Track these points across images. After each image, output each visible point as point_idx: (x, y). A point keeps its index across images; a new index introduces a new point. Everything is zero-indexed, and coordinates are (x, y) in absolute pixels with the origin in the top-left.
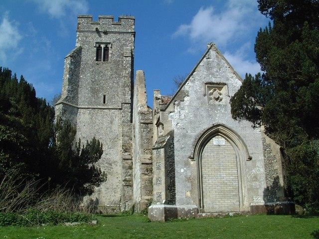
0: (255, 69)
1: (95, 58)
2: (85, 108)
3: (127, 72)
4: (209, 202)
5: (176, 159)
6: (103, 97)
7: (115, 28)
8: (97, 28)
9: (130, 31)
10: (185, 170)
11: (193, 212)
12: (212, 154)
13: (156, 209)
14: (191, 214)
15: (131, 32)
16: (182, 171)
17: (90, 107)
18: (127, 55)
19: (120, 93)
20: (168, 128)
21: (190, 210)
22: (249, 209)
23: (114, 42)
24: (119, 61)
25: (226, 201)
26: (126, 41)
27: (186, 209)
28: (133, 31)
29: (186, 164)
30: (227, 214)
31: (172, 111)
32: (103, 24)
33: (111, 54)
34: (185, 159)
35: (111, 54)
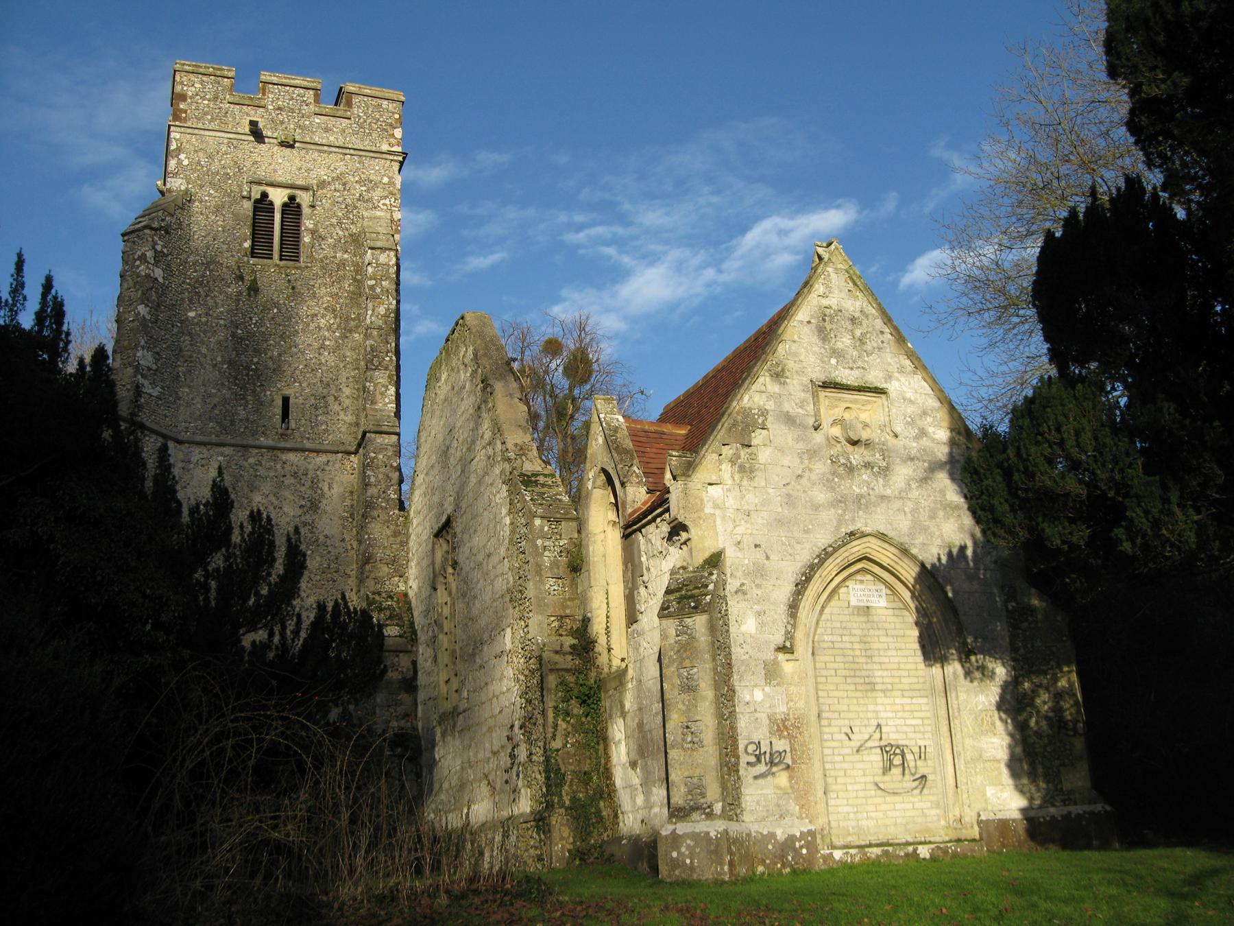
0: (1048, 345)
1: (247, 244)
2: (205, 444)
3: (382, 310)
4: (846, 809)
5: (737, 652)
6: (279, 402)
7: (327, 130)
8: (253, 124)
9: (385, 148)
10: (766, 695)
11: (801, 847)
12: (846, 639)
13: (695, 836)
14: (797, 852)
15: (390, 153)
16: (758, 695)
17: (229, 439)
18: (379, 244)
19: (347, 391)
20: (704, 541)
21: (791, 839)
22: (975, 833)
23: (322, 184)
24: (343, 264)
25: (898, 806)
26: (371, 185)
27: (781, 835)
28: (399, 149)
29: (771, 673)
30: (910, 849)
31: (714, 479)
32: (279, 109)
33: (313, 232)
34: (769, 655)
35: (313, 232)
